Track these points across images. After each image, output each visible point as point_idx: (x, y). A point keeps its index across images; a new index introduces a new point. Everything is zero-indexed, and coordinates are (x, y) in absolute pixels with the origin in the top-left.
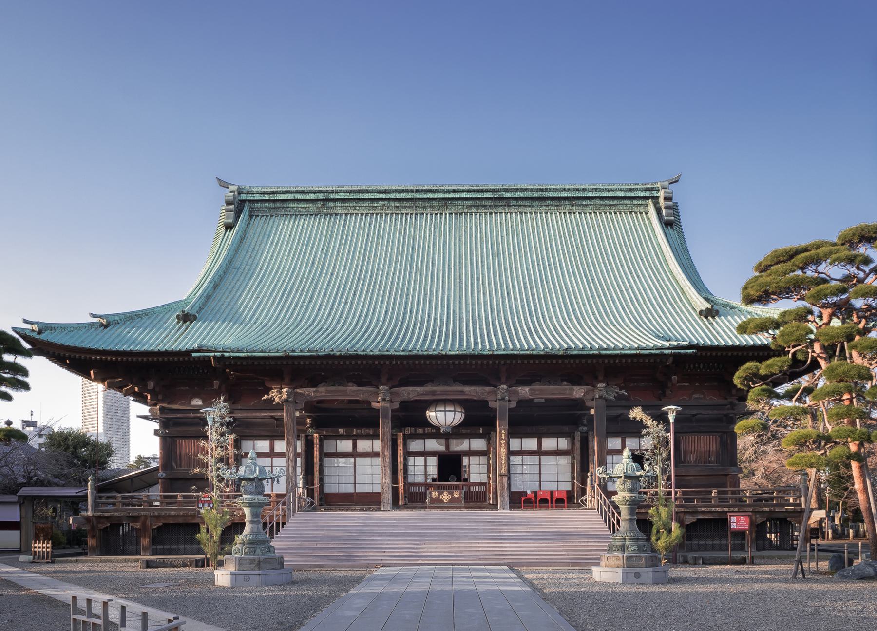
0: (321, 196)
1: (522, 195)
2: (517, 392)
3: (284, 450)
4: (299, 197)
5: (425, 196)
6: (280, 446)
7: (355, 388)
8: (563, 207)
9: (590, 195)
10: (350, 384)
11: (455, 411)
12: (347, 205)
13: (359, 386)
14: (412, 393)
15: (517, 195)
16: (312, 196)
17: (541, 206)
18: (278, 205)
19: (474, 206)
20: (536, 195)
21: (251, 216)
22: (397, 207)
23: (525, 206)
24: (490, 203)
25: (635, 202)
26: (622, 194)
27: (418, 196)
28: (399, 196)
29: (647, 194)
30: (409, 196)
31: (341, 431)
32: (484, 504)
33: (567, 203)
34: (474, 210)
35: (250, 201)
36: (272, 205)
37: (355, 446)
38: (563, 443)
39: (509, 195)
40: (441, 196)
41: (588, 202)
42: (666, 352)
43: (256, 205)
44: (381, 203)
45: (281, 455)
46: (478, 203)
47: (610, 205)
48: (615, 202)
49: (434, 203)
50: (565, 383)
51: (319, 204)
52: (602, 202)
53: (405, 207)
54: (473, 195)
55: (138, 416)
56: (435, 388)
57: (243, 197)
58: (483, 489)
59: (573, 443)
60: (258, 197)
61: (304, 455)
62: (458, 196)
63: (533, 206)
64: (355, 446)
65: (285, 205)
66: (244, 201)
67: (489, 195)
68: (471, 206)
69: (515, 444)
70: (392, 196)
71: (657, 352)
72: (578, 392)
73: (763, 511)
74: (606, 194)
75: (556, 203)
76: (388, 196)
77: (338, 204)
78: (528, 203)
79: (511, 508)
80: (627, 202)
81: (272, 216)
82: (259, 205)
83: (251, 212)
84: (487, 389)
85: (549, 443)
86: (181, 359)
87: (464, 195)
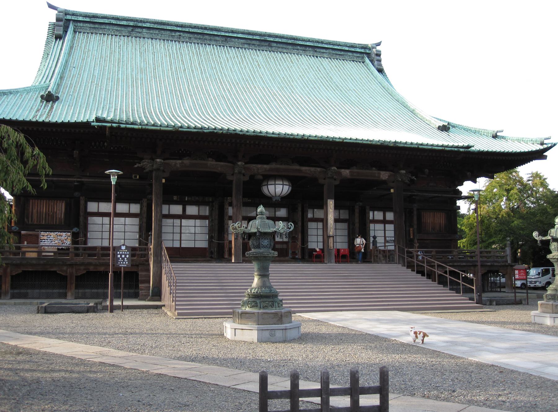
0: (131, 24)
1: (280, 40)
2: (340, 174)
3: (207, 214)
4: (114, 22)
5: (211, 33)
6: (390, 216)
7: (214, 163)
8: (308, 52)
9: (326, 46)
10: (210, 159)
11: (283, 185)
12: (151, 32)
13: (216, 161)
14: (260, 168)
15: (277, 40)
16: (124, 23)
17: (294, 49)
18: (97, 26)
19: (247, 44)
20: (290, 42)
21: (75, 32)
22: (190, 38)
23: (283, 48)
24: (258, 43)
25: (355, 54)
26: (347, 49)
27: (206, 32)
28: (191, 30)
29: (362, 51)
30: (199, 31)
31: (175, 198)
32: (287, 258)
33: (310, 49)
34: (246, 46)
35: (74, 21)
36: (92, 26)
37: (184, 210)
38: (206, 211)
39: (272, 39)
40: (223, 34)
41: (324, 51)
42: (461, 150)
43: (79, 24)
44: (178, 34)
45: (390, 222)
46: (249, 42)
47: (340, 55)
48: (342, 53)
49: (217, 38)
50: (374, 169)
51: (130, 29)
52: (333, 52)
53: (196, 38)
54: (246, 36)
55: (555, 145)
56: (278, 166)
57: (69, 17)
58: (285, 246)
59: (211, 211)
60: (80, 19)
61: (226, 218)
62: (235, 35)
63: (288, 49)
64: (184, 210)
65: (103, 27)
66: (69, 20)
67: (257, 38)
68: (245, 44)
69: (165, 209)
70: (187, 30)
71: (456, 149)
72: (384, 175)
73: (487, 265)
74: (336, 47)
75: (304, 48)
76: (184, 29)
77: (145, 30)
78: (284, 46)
79: (336, 262)
80: (350, 54)
81: (92, 33)
82: (81, 24)
83: (74, 29)
84: (319, 169)
85: (192, 210)
86: (45, 129)
87: (240, 36)
